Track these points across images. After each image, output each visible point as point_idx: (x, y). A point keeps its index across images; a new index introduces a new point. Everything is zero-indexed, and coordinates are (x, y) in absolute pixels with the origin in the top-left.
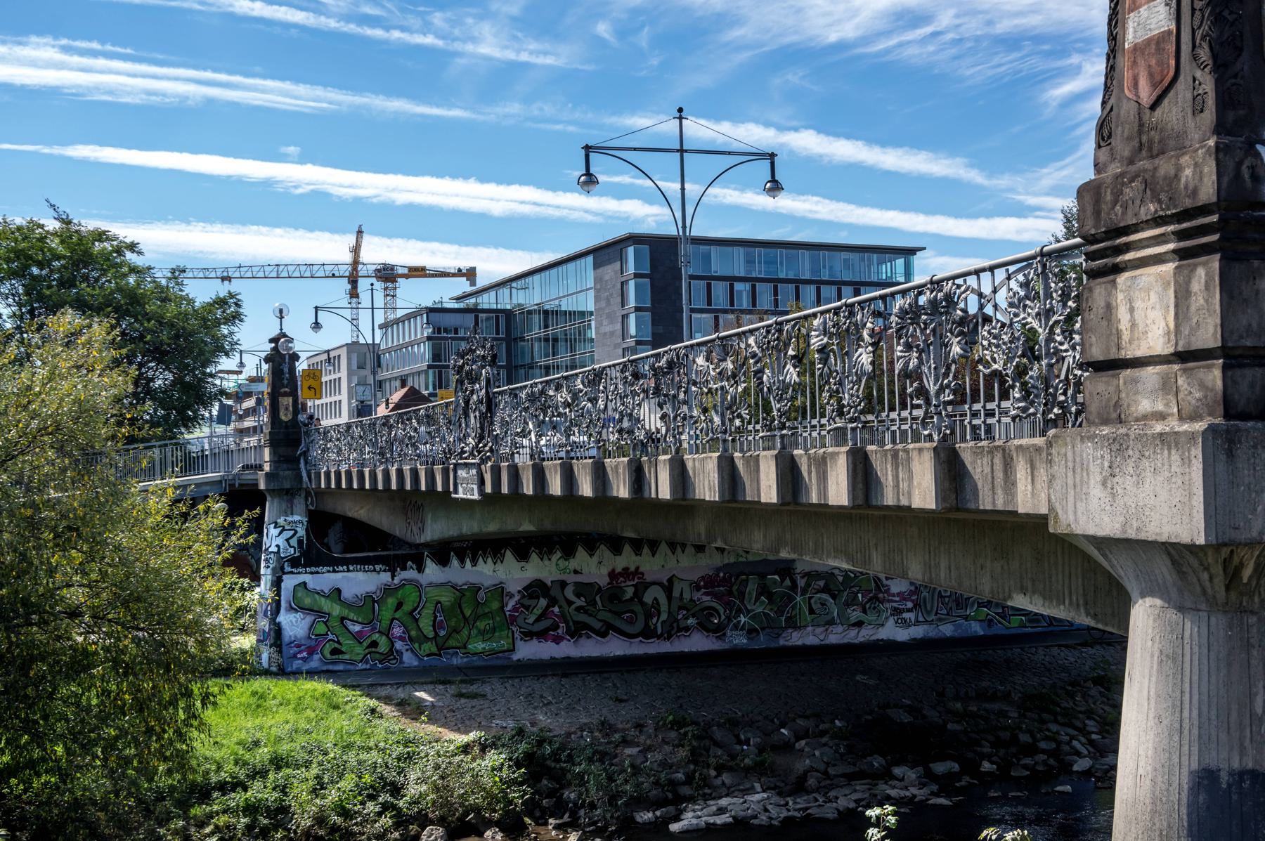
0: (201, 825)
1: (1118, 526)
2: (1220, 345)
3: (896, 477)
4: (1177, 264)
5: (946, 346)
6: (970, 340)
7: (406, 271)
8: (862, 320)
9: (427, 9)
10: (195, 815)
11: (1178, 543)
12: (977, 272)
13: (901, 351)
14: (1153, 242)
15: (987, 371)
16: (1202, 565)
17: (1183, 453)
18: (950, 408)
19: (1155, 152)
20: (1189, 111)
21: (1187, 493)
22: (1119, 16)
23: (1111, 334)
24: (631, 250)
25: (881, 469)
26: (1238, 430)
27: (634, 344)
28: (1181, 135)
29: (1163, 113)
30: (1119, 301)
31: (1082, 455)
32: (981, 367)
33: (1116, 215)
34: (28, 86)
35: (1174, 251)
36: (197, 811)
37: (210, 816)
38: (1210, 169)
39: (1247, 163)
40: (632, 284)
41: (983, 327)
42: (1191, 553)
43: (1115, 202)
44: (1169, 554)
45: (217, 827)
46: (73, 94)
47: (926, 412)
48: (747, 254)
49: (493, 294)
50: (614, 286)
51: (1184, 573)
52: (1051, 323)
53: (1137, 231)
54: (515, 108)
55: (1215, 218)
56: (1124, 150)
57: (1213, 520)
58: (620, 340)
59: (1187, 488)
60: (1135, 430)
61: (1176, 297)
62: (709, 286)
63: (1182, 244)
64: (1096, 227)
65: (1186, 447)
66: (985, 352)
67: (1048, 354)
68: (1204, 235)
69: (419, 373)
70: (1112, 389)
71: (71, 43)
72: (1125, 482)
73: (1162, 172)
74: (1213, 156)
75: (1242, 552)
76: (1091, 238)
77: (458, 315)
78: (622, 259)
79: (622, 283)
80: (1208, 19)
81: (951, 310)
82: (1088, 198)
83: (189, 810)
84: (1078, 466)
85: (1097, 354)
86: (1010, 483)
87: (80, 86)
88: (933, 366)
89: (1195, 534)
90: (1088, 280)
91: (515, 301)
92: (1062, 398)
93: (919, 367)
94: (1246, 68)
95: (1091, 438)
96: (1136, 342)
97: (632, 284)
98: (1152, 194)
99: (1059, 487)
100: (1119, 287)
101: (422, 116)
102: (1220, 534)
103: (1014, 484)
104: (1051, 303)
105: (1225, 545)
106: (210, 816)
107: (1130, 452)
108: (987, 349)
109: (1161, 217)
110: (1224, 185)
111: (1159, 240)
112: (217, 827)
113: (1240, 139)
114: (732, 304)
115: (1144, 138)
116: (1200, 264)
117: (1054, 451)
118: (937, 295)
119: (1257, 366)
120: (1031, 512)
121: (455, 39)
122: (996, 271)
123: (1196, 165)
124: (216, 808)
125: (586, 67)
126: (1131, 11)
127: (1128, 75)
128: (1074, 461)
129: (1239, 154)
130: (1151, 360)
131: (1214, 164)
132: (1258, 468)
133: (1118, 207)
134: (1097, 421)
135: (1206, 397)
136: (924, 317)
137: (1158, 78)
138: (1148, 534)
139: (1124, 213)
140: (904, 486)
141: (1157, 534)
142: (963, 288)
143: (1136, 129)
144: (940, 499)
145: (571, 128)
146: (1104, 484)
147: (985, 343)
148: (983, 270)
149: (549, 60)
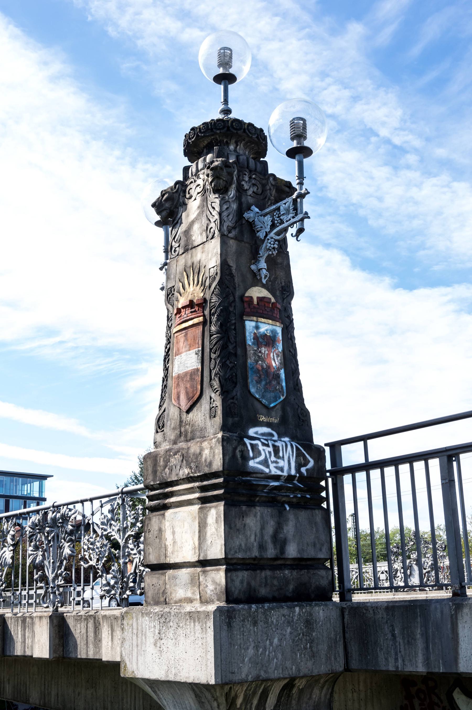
1: (163, 672)
2: (224, 557)
3: (24, 636)
4: (200, 506)
5: (61, 548)
6: (75, 542)
8: (7, 529)
11: (199, 684)
12: (82, 502)
13: (32, 551)
14: (186, 492)
15: (86, 566)
16: (213, 697)
17: (202, 624)
18: (61, 589)
19: (188, 438)
20: (208, 416)
21: (204, 651)
22: (170, 357)
23: (161, 547)
25: (14, 630)
26: (234, 610)
28: (203, 429)
29: (193, 416)
30: (166, 527)
31: (142, 626)
32: (82, 563)
33: (166, 474)
35: (199, 498)
38: (219, 450)
39: (239, 449)
41: (84, 537)
42: (207, 689)
43: (165, 467)
44: (194, 690)
47: (46, 592)
51: (203, 702)
52: (126, 536)
53: (177, 485)
55: (221, 480)
56: (171, 435)
57: (219, 668)
59: (204, 647)
60: (174, 609)
61: (199, 526)
63: (203, 494)
64: (154, 480)
65: (204, 621)
66: (85, 553)
67: (124, 556)
68: (216, 489)
70: (161, 582)
72: (168, 643)
73: (192, 450)
74: (221, 444)
75: (237, 688)
76: (150, 487)
80: (218, 365)
81: (64, 525)
82: (149, 462)
84: (140, 632)
85: (153, 560)
86: (98, 640)
88: (52, 561)
89: (209, 677)
90: (149, 502)
92: (131, 585)
93: (42, 561)
95: (148, 614)
96: (176, 553)
98: (186, 463)
99: (128, 646)
100: (167, 518)
102: (223, 679)
103: (100, 641)
104: (127, 523)
105: (227, 684)
107: (171, 624)
108: (87, 551)
109: (191, 477)
110: (227, 461)
111: (190, 491)
113: (235, 434)
115: (183, 429)
116: (213, 507)
117: (125, 622)
118: (56, 515)
119: (244, 570)
120: (110, 660)
122: (94, 501)
123: (211, 448)
126: (177, 355)
127: (174, 392)
128: (137, 629)
129: (235, 443)
130: (185, 564)
131: (221, 448)
132: (245, 634)
133: (167, 470)
134: (152, 602)
135: (216, 589)
136: (47, 529)
137: (191, 395)
138: (181, 678)
139: (170, 473)
140: (28, 641)
141: (187, 678)
142: (73, 512)
143: (178, 423)
144: (52, 651)
146: (155, 644)
147: (86, 547)
148: (86, 500)
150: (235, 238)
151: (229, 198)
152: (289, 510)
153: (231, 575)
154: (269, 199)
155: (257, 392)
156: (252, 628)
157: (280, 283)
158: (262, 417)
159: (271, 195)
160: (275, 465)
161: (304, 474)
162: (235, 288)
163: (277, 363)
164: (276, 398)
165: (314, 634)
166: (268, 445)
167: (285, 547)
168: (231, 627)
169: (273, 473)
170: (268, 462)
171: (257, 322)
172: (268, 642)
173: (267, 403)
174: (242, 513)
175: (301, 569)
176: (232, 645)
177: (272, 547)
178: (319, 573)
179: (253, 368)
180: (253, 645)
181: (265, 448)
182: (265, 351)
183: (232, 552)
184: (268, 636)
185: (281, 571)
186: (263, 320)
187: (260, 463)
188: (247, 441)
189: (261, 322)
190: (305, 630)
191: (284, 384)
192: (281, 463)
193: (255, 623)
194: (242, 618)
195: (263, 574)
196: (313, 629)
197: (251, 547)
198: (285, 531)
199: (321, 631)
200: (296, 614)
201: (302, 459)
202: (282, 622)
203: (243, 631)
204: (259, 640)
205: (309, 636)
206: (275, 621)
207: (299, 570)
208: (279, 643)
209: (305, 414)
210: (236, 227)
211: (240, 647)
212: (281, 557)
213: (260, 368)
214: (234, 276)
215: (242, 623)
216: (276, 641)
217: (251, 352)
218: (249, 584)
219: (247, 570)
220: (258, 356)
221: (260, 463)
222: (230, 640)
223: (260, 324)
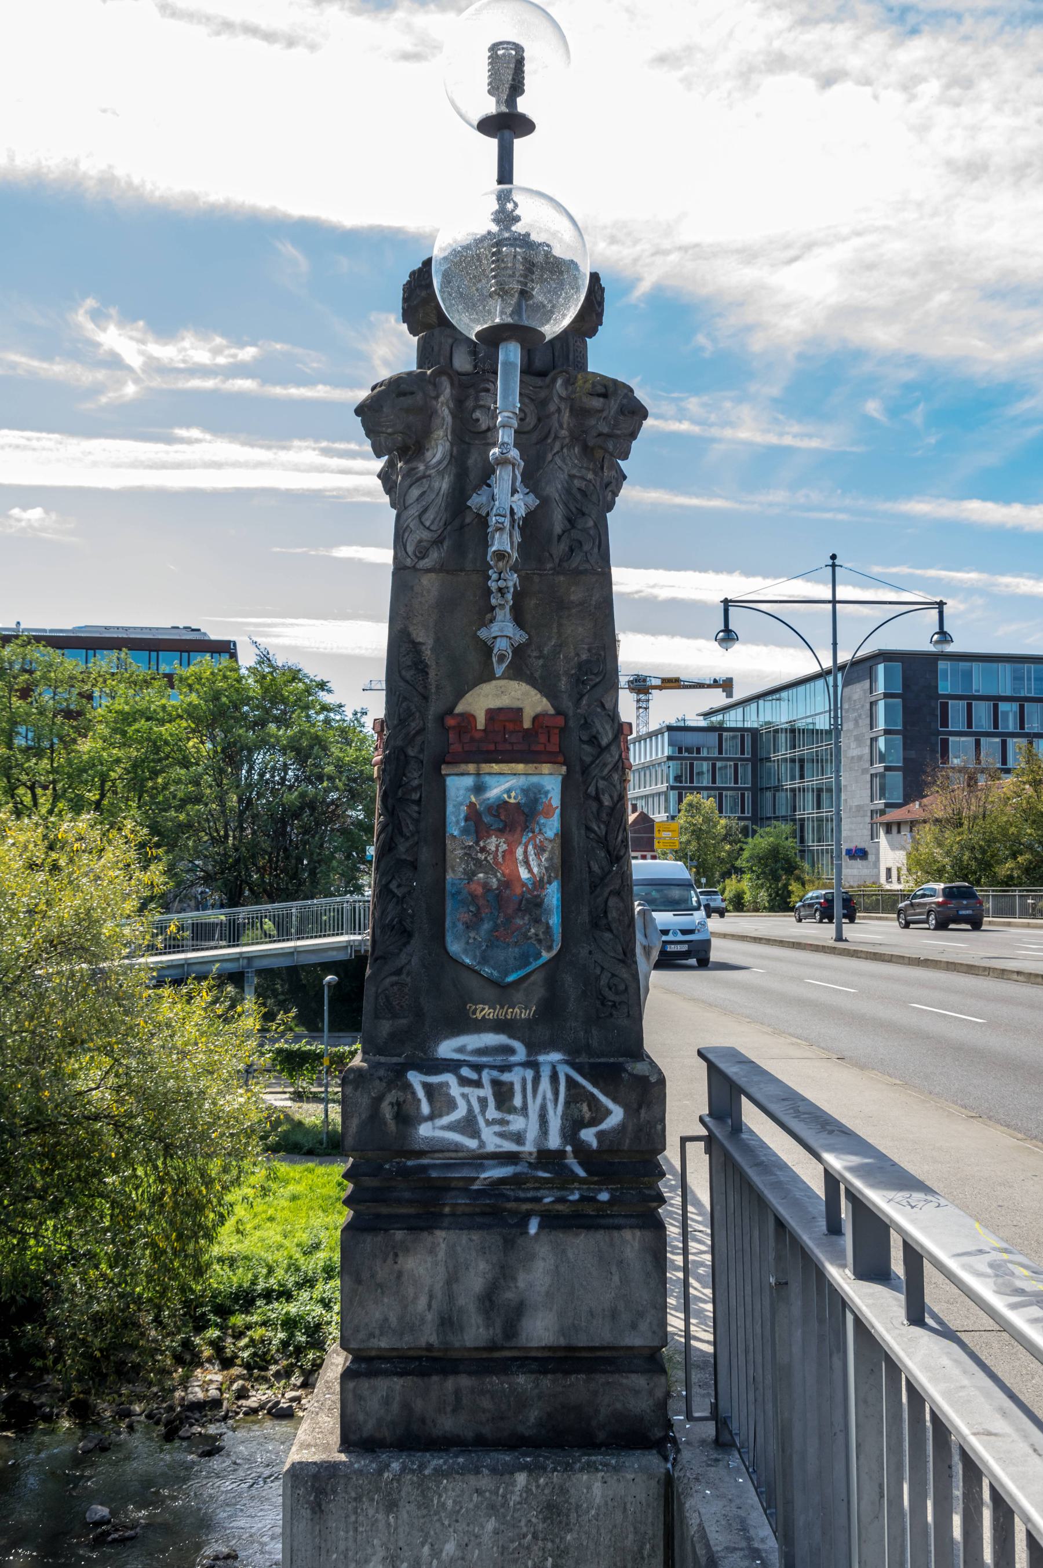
0: (239, 1335)
7: (658, 682)
9: (681, 395)
10: (234, 1325)
24: (881, 668)
27: (882, 770)
34: (292, 490)
36: (238, 1320)
37: (249, 1327)
39: (391, 1097)
40: (881, 704)
45: (252, 1340)
46: (334, 497)
48: (1015, 671)
49: (740, 710)
50: (863, 706)
54: (779, 496)
58: (867, 765)
62: (969, 706)
69: (659, 794)
71: (331, 445)
77: (701, 734)
78: (872, 677)
79: (871, 703)
83: (228, 1319)
87: (339, 489)
91: (761, 719)
94: (415, 961)
97: (881, 704)
101: (681, 507)
106: (249, 1327)
112: (252, 1340)
114: (996, 726)
121: (711, 425)
124: (255, 1318)
125: (855, 449)
132: (360, 1529)
145: (841, 516)
149: (814, 443)
150: (440, 569)
151: (427, 468)
152: (537, 1234)
153: (355, 1388)
154: (556, 437)
155: (466, 951)
156: (380, 1516)
157: (572, 654)
158: (483, 1009)
159: (561, 426)
160: (497, 1128)
161: (590, 1146)
162: (425, 698)
163: (535, 870)
164: (524, 960)
165: (569, 1537)
166: (478, 1084)
167: (519, 1320)
168: (322, 1511)
169: (490, 1148)
170: (477, 1123)
171: (478, 775)
172: (426, 1549)
173: (495, 973)
174: (394, 1247)
175: (567, 1373)
176: (323, 1552)
177: (480, 1321)
178: (624, 1381)
179: (459, 892)
180: (381, 1553)
181: (467, 1090)
182: (497, 846)
183: (362, 1335)
184: (427, 1535)
185: (503, 1378)
186: (496, 767)
187: (451, 1127)
188: (415, 1078)
189: (490, 774)
190: (541, 1526)
191: (555, 920)
192: (517, 1123)
193: (392, 1506)
194: (353, 1495)
195: (450, 1383)
196: (567, 1524)
197: (417, 1323)
198: (521, 1284)
199: (594, 1531)
200: (518, 1488)
201: (585, 1108)
202: (471, 1506)
203: (356, 1522)
204: (401, 1544)
205: (553, 1541)
206: (450, 1503)
207: (559, 1376)
208: (459, 1554)
209: (622, 987)
210: (444, 538)
211: (346, 1557)
212: (507, 1345)
213: (480, 890)
214: (427, 666)
215: (354, 1504)
216: (450, 1548)
217: (455, 853)
218: (406, 1406)
219: (401, 1374)
220: (477, 859)
221: (451, 1127)
222: (317, 1540)
223: (487, 779)
